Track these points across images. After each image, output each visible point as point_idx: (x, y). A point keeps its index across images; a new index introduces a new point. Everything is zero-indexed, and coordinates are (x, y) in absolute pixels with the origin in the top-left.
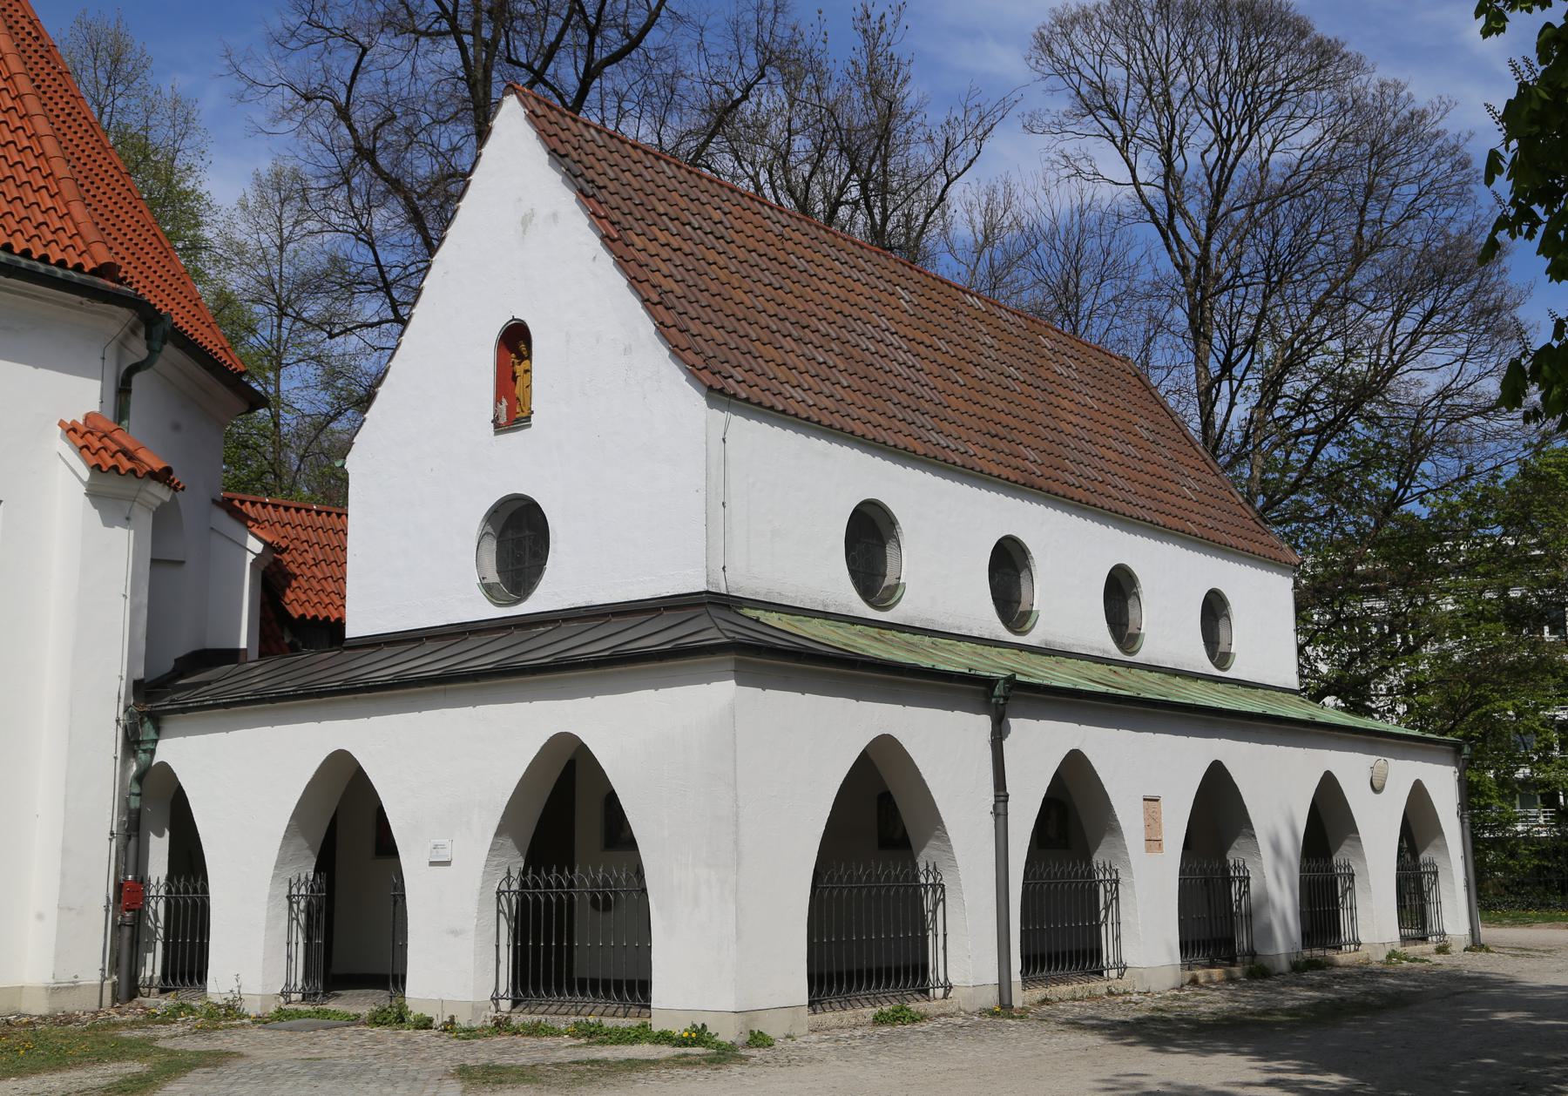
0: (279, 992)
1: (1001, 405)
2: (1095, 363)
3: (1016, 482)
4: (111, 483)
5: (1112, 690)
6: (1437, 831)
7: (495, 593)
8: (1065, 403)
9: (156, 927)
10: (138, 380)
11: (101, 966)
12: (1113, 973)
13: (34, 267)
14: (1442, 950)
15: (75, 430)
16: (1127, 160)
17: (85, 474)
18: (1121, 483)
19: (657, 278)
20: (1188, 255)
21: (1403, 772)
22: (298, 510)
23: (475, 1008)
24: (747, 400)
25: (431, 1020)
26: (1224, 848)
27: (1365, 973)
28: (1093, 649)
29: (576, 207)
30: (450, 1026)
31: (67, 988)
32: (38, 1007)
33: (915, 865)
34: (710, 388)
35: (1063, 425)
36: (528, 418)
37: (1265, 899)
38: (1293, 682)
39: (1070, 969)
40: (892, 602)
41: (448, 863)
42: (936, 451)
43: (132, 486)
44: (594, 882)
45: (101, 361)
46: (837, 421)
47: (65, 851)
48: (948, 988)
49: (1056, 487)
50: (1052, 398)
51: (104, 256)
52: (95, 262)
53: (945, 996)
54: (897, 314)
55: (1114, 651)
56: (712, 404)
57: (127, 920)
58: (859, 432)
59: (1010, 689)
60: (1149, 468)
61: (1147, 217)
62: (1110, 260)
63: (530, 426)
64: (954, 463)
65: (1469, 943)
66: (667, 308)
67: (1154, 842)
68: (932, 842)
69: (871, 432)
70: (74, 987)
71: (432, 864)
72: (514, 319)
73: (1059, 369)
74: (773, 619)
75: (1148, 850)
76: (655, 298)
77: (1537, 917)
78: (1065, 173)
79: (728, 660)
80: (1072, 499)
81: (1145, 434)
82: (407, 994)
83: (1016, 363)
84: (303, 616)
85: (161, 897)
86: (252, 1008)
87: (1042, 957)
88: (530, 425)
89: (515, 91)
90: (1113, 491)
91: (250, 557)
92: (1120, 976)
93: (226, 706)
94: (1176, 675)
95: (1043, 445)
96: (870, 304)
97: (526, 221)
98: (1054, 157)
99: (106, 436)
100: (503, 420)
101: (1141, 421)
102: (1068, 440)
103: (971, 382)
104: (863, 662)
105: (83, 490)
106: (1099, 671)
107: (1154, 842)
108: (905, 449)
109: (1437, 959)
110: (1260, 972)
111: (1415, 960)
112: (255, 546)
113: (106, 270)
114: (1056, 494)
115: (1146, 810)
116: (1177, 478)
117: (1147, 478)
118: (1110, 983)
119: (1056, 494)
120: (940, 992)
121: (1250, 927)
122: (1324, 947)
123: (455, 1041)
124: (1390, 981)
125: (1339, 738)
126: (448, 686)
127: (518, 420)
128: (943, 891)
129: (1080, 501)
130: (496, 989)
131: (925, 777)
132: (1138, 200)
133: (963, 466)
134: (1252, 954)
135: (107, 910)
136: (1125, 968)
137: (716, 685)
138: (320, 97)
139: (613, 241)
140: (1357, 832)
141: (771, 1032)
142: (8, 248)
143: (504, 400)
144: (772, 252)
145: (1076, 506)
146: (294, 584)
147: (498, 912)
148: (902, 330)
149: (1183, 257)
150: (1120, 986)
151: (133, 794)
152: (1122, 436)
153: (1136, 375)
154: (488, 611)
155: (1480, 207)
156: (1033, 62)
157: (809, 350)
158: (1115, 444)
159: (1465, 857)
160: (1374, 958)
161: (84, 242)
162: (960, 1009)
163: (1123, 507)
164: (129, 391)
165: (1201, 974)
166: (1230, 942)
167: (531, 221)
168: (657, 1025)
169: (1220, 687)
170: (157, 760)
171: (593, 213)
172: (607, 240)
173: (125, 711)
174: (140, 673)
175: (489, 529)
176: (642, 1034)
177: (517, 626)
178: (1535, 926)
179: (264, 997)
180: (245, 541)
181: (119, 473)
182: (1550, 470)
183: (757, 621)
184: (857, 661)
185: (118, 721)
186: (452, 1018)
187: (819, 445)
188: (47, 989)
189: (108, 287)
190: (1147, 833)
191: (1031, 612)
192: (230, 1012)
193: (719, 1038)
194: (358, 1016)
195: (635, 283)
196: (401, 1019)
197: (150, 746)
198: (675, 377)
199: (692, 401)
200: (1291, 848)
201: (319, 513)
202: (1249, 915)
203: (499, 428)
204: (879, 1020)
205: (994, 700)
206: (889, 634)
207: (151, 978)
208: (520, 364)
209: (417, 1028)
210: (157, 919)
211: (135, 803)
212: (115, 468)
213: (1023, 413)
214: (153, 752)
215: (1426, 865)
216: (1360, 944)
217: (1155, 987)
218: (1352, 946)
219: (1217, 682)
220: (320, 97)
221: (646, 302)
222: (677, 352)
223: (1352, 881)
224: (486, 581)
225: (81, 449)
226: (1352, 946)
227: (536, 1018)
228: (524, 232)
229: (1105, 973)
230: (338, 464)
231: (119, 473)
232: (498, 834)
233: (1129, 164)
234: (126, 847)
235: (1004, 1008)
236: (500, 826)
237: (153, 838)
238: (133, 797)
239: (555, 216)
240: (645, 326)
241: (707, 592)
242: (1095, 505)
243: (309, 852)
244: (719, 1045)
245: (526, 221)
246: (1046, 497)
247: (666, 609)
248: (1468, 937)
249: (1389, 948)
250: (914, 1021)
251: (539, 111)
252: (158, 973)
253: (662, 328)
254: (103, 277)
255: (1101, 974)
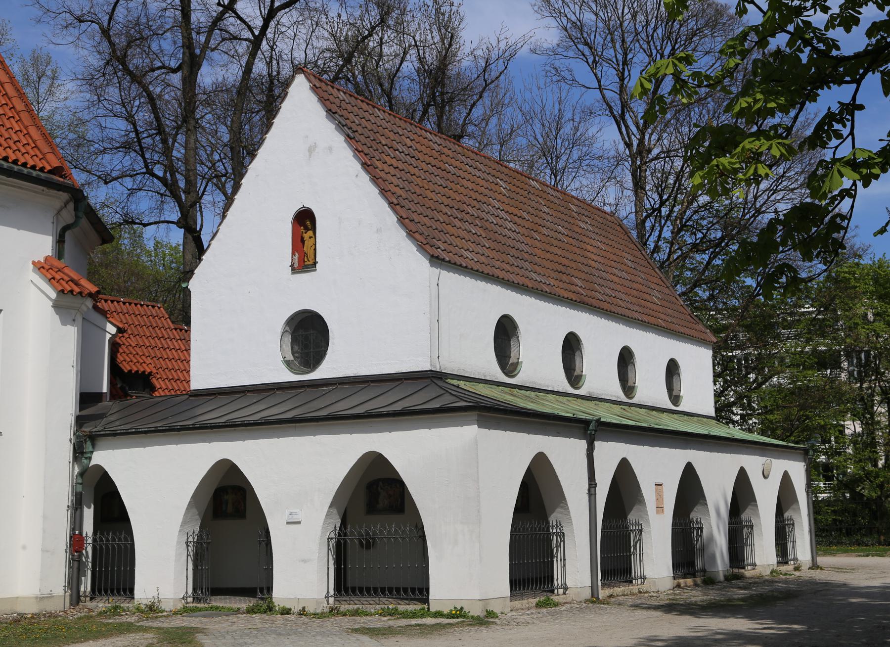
0: (182, 597)
1: (559, 252)
2: (598, 218)
3: (576, 301)
4: (69, 299)
5: (638, 424)
6: (795, 500)
7: (293, 366)
8: (589, 247)
9: (87, 561)
10: (68, 235)
11: (64, 584)
12: (561, 591)
13: (11, 167)
14: (797, 569)
15: (43, 267)
16: (595, 75)
17: (53, 295)
18: (623, 297)
19: (394, 189)
20: (633, 137)
21: (780, 466)
22: (112, 302)
23: (318, 602)
24: (449, 262)
25: (290, 609)
26: (690, 510)
27: (760, 581)
28: (612, 396)
29: (345, 145)
30: (303, 613)
31: (47, 597)
32: (30, 609)
33: (548, 522)
34: (432, 256)
35: (591, 262)
36: (315, 263)
37: (711, 538)
38: (714, 415)
39: (524, 589)
40: (516, 373)
41: (299, 523)
42: (536, 285)
43: (79, 300)
44: (360, 534)
45: (51, 225)
46: (487, 270)
47: (45, 517)
48: (566, 588)
49: (594, 302)
50: (582, 244)
51: (56, 163)
52: (50, 165)
53: (564, 593)
54: (499, 197)
55: (622, 397)
56: (432, 264)
57: (76, 557)
58: (501, 277)
59: (598, 426)
60: (635, 286)
61: (607, 112)
62: (578, 134)
63: (316, 270)
64: (546, 292)
65: (811, 565)
66: (402, 207)
67: (660, 509)
68: (558, 510)
69: (507, 276)
70: (50, 597)
71: (288, 523)
72: (304, 207)
73: (583, 225)
74: (462, 384)
75: (658, 513)
76: (395, 202)
77: (838, 550)
78: (555, 79)
79: (474, 415)
80: (603, 309)
81: (630, 264)
82: (274, 595)
83: (562, 223)
84: (130, 371)
85: (332, 538)
86: (167, 606)
87: (532, 579)
88: (316, 270)
89: (303, 72)
90: (620, 303)
91: (108, 336)
92: (643, 583)
93: (146, 432)
94: (653, 410)
95: (583, 276)
96: (486, 192)
97: (311, 150)
98: (548, 68)
99: (59, 271)
100: (296, 266)
101: (626, 255)
102: (594, 271)
103: (544, 239)
104: (534, 414)
105: (51, 304)
106: (617, 409)
107: (660, 509)
108: (523, 285)
109: (797, 573)
110: (709, 581)
111: (786, 574)
112: (111, 329)
113: (56, 171)
114: (595, 307)
115: (656, 490)
116: (649, 291)
117: (635, 293)
118: (639, 587)
119: (595, 307)
120: (561, 591)
121: (703, 556)
122: (739, 568)
123: (314, 619)
124: (780, 585)
125: (747, 447)
126: (298, 424)
127: (307, 267)
128: (564, 535)
129: (607, 310)
130: (328, 592)
131: (558, 474)
132: (602, 101)
133: (550, 293)
134: (704, 571)
135: (66, 552)
136: (646, 578)
137: (466, 428)
138: (90, 21)
139: (368, 166)
140: (756, 502)
141: (497, 611)
142: (6, 159)
143: (296, 254)
144: (434, 162)
145: (604, 313)
146: (121, 350)
147: (188, 555)
148: (507, 208)
149: (629, 138)
150: (644, 588)
151: (78, 483)
152: (619, 266)
153: (620, 225)
154: (289, 377)
155: (809, 113)
156: (536, 8)
157: (466, 226)
158: (616, 272)
159: (809, 515)
160: (764, 574)
161: (41, 152)
162: (573, 600)
163: (627, 313)
164: (64, 242)
165: (682, 581)
166: (692, 564)
167: (314, 150)
168: (433, 608)
169: (675, 416)
170: (93, 463)
171: (356, 150)
172: (365, 166)
173: (74, 434)
174: (78, 413)
175: (287, 328)
176: (428, 613)
177: (309, 386)
178: (838, 555)
179: (175, 600)
180: (106, 327)
181: (72, 294)
182: (846, 275)
183: (458, 387)
184: (530, 413)
185: (70, 440)
186: (304, 608)
187: (481, 284)
188: (36, 598)
189: (58, 181)
190: (657, 504)
191: (581, 376)
192: (152, 609)
193: (471, 614)
194: (239, 609)
195: (383, 192)
196: (270, 609)
197: (89, 455)
198: (409, 248)
199: (421, 262)
200: (725, 512)
201: (124, 303)
202: (703, 549)
203: (294, 270)
204: (539, 605)
205: (589, 432)
206: (515, 391)
207: (85, 592)
208: (306, 233)
209: (282, 614)
210: (87, 557)
211: (79, 488)
212: (72, 291)
213: (570, 256)
214: (90, 458)
215: (788, 520)
216: (756, 565)
217: (662, 589)
218: (639, 580)
219: (674, 413)
220: (90, 21)
221: (391, 204)
222: (411, 234)
223: (752, 529)
224: (286, 359)
225: (50, 280)
226: (639, 580)
227: (356, 607)
228: (310, 156)
229: (556, 591)
230: (184, 285)
231: (72, 294)
232: (330, 507)
233: (597, 78)
234: (75, 513)
235: (594, 599)
236: (332, 502)
237: (85, 509)
238: (78, 485)
239: (330, 149)
240: (390, 218)
241: (431, 371)
242: (614, 313)
243: (198, 517)
244: (472, 617)
245: (311, 150)
246: (589, 309)
247: (405, 379)
248: (810, 562)
249: (771, 568)
250: (555, 606)
251: (318, 85)
252: (89, 589)
253: (401, 220)
254: (54, 174)
255: (631, 582)
